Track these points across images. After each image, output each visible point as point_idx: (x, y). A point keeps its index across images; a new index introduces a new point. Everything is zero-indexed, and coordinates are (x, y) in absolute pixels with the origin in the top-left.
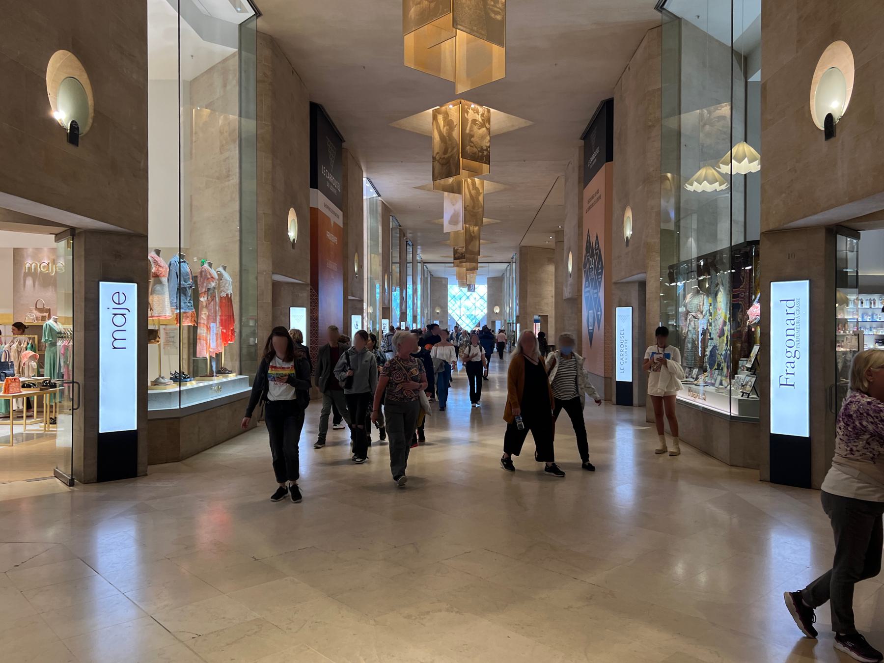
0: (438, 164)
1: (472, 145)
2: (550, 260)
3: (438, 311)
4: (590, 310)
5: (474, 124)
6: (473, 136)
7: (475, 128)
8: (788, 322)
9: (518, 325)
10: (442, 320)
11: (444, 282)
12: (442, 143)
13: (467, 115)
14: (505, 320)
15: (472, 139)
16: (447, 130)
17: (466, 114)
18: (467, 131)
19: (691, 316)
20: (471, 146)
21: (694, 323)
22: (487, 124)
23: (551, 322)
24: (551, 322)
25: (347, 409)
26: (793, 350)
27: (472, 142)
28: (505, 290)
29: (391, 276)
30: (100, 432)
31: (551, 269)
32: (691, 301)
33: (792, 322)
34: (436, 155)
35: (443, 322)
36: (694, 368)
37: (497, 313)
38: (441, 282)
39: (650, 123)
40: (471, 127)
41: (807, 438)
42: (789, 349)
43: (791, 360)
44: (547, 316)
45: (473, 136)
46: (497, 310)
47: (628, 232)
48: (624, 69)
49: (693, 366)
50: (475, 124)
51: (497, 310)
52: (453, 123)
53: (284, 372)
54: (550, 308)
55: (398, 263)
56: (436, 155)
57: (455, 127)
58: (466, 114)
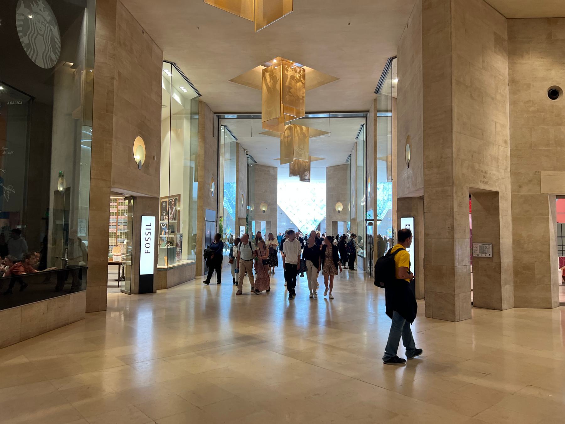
1: (291, 94)
5: (293, 79)
6: (291, 88)
7: (293, 82)
11: (272, 172)
12: (269, 93)
13: (287, 72)
15: (291, 90)
16: (272, 83)
17: (286, 72)
18: (287, 84)
20: (290, 96)
22: (303, 79)
27: (291, 93)
30: (141, 274)
37: (339, 211)
38: (269, 171)
40: (290, 82)
44: (497, 193)
45: (291, 88)
46: (340, 207)
50: (294, 79)
51: (340, 207)
52: (276, 78)
54: (503, 171)
57: (278, 81)
58: (286, 72)
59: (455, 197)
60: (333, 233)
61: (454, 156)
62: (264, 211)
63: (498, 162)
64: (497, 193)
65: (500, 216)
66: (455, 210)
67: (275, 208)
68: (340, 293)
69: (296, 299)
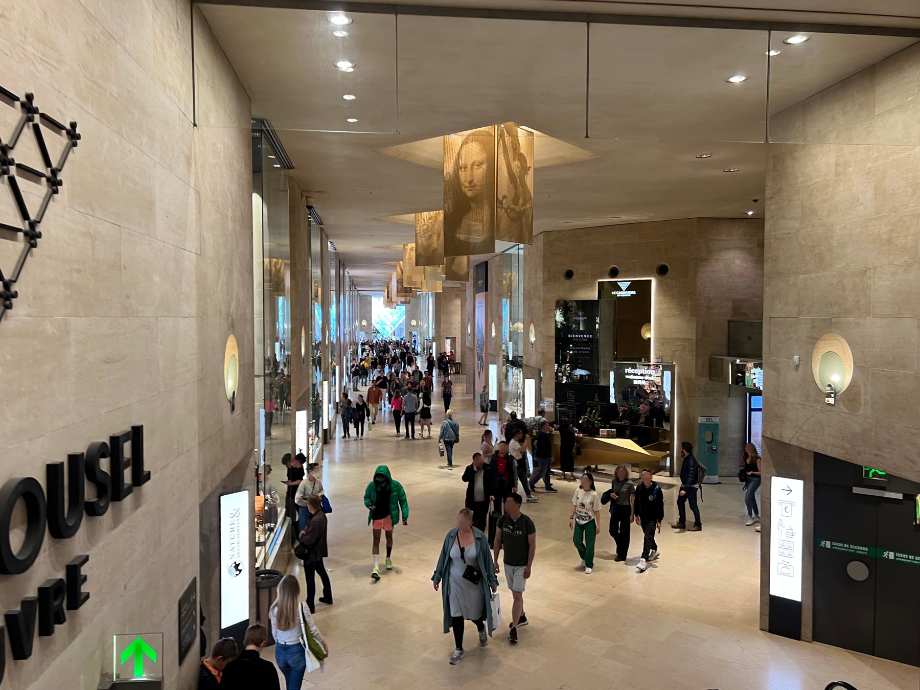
2: (457, 296)
4: (515, 351)
10: (367, 331)
14: (424, 337)
23: (458, 341)
24: (458, 341)
25: (619, 532)
28: (421, 309)
31: (458, 302)
46: (414, 323)
47: (494, 334)
48: (823, 89)
51: (414, 323)
55: (469, 257)
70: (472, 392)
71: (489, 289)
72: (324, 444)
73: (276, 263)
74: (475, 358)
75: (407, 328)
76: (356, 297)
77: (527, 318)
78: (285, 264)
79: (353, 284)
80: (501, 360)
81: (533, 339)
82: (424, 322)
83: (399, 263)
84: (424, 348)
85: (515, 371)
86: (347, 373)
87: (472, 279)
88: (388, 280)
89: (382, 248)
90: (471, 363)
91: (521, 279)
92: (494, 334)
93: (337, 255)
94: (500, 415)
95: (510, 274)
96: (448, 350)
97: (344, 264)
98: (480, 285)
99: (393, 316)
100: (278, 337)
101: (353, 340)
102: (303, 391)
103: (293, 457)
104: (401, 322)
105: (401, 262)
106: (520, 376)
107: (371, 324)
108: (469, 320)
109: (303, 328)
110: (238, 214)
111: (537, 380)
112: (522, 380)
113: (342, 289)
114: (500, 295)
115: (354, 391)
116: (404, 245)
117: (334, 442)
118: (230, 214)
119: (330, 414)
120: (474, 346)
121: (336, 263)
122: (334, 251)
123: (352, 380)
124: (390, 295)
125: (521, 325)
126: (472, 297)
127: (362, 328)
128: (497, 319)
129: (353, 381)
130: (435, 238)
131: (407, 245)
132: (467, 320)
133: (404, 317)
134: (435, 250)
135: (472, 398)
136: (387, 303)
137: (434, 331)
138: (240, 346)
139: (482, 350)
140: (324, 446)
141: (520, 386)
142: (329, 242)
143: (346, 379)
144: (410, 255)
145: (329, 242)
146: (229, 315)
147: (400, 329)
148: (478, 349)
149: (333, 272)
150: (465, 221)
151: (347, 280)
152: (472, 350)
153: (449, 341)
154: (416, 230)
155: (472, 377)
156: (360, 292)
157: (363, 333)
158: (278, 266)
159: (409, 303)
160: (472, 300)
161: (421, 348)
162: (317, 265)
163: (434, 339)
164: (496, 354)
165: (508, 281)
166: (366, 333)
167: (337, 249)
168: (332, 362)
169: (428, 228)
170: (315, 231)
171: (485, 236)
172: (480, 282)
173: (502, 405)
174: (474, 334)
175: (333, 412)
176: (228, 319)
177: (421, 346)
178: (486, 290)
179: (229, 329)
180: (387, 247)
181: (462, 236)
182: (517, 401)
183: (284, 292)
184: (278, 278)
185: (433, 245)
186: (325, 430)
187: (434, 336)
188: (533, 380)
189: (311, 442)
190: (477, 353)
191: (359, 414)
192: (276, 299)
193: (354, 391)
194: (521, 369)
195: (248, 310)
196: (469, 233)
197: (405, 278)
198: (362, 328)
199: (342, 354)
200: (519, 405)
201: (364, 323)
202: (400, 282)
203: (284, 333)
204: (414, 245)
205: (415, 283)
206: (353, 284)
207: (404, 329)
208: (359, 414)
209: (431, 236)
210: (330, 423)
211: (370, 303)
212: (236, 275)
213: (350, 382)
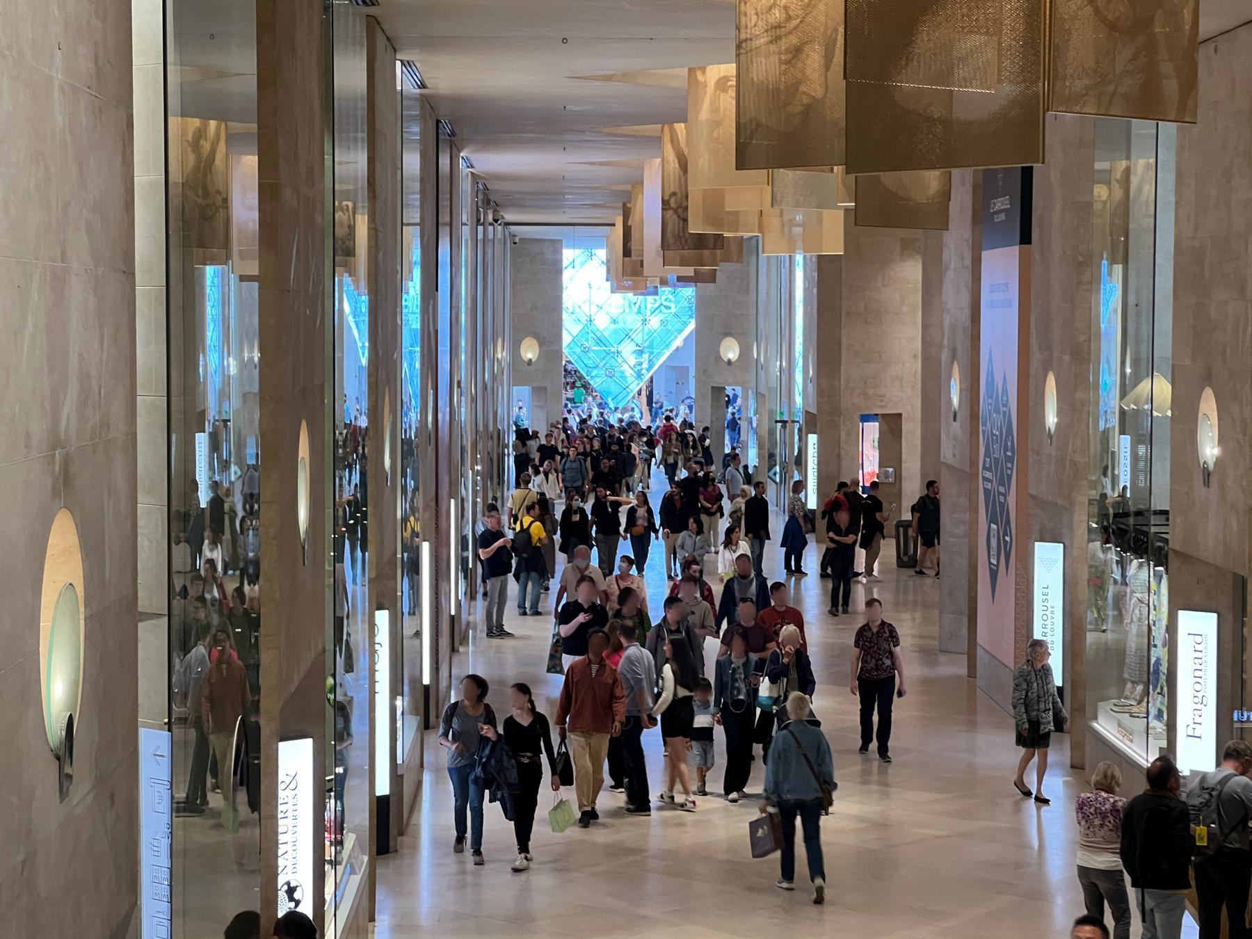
0: (675, 216)
3: (530, 356)
8: (1196, 661)
9: (813, 439)
10: (541, 384)
14: (771, 412)
19: (1135, 599)
21: (1140, 611)
26: (1200, 695)
28: (762, 296)
29: (432, 302)
31: (911, 272)
32: (1135, 575)
33: (1200, 661)
34: (670, 198)
35: (545, 388)
36: (1138, 684)
39: (1081, 259)
41: (516, 825)
42: (1196, 694)
43: (1199, 707)
44: (900, 415)
46: (730, 351)
47: (1051, 420)
49: (1137, 680)
51: (730, 351)
53: (781, 771)
56: (670, 198)
59: (842, 426)
60: (714, 419)
61: (842, 387)
62: (530, 360)
63: (902, 381)
64: (900, 415)
65: (903, 439)
66: (842, 440)
67: (557, 351)
68: (862, 819)
69: (597, 584)
70: (964, 646)
71: (1035, 235)
72: (378, 854)
73: (200, 134)
74: (975, 510)
75: (703, 372)
76: (498, 248)
77: (1188, 362)
78: (231, 138)
79: (487, 202)
80: (1083, 521)
81: (1210, 451)
82: (773, 349)
83: (673, 132)
84: (772, 456)
85: (1139, 572)
86: (463, 561)
87: (968, 188)
88: (629, 187)
89: (609, 78)
90: (961, 530)
91: (1168, 179)
92: (1051, 420)
93: (429, 104)
94: (1077, 747)
95: (1124, 163)
96: (869, 466)
97: (453, 134)
98: (1002, 217)
99: (645, 321)
100: (204, 411)
101: (486, 426)
102: (304, 666)
103: (266, 926)
104: (678, 342)
105: (680, 127)
106: (1158, 593)
107: (558, 353)
108: (953, 356)
109: (304, 424)
110: (85, 64)
111: (1229, 617)
112: (1165, 609)
113: (445, 217)
114: (1080, 265)
115: (490, 634)
116: (690, 70)
117: (415, 847)
118: (58, 77)
119: (399, 734)
120: (974, 463)
121: (423, 134)
122: (418, 91)
123: (481, 590)
124: (634, 246)
125: (1162, 388)
126: (968, 262)
127: (521, 371)
128: (1067, 358)
129: (485, 594)
130: (814, 59)
131: (703, 70)
132: (945, 355)
133: (692, 325)
134: (812, 108)
135: (963, 670)
136: (624, 273)
137: (811, 389)
138: (91, 547)
139: (1004, 481)
140: (381, 861)
141: (1159, 633)
142: (398, 64)
143: (456, 587)
144: (715, 109)
145: (398, 64)
146: (55, 442)
147: (674, 370)
148: (988, 475)
149: (412, 162)
150: (926, 38)
151: (465, 187)
152: (968, 476)
153: (872, 430)
154: (738, 28)
155: (964, 582)
156: (513, 228)
157: (522, 393)
158: (206, 146)
159: (714, 281)
160: (967, 276)
161: (760, 456)
162: (356, 139)
163: (811, 423)
164: (1060, 501)
165: (1118, 193)
166: (539, 391)
167: (427, 83)
168: (405, 520)
169: (789, 18)
170: (348, 25)
171: (1008, 90)
172: (1002, 203)
173: (1085, 712)
174: (974, 415)
175: (409, 728)
176: (53, 456)
177: (760, 447)
178: (1026, 238)
179: (55, 494)
180: (625, 77)
181: (908, 84)
182: (1146, 693)
183: (226, 244)
184: (206, 194)
185: (803, 88)
186: (380, 798)
187: (813, 410)
188: (1213, 617)
189: (330, 852)
190: (985, 490)
191: (520, 764)
192: (196, 272)
193: (490, 634)
194: (1161, 568)
195: (117, 409)
196: (945, 75)
197: (696, 191)
198: (521, 371)
199: (444, 492)
200: (1153, 712)
201: (530, 351)
202: (676, 206)
203: (223, 394)
204: (730, 69)
205: (735, 220)
206: (487, 202)
207: (692, 371)
208: (520, 764)
209: (797, 51)
210: (396, 777)
211: (556, 270)
212: (78, 288)
213: (472, 596)
